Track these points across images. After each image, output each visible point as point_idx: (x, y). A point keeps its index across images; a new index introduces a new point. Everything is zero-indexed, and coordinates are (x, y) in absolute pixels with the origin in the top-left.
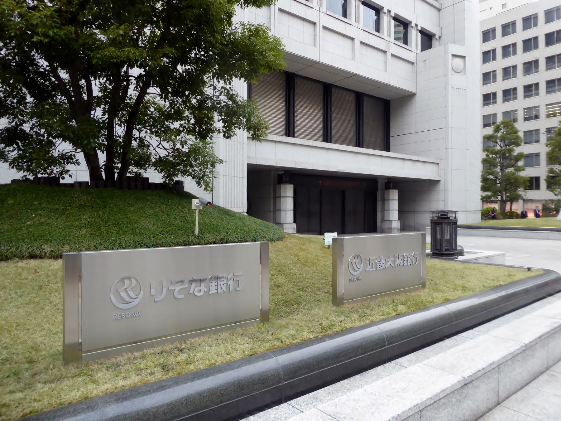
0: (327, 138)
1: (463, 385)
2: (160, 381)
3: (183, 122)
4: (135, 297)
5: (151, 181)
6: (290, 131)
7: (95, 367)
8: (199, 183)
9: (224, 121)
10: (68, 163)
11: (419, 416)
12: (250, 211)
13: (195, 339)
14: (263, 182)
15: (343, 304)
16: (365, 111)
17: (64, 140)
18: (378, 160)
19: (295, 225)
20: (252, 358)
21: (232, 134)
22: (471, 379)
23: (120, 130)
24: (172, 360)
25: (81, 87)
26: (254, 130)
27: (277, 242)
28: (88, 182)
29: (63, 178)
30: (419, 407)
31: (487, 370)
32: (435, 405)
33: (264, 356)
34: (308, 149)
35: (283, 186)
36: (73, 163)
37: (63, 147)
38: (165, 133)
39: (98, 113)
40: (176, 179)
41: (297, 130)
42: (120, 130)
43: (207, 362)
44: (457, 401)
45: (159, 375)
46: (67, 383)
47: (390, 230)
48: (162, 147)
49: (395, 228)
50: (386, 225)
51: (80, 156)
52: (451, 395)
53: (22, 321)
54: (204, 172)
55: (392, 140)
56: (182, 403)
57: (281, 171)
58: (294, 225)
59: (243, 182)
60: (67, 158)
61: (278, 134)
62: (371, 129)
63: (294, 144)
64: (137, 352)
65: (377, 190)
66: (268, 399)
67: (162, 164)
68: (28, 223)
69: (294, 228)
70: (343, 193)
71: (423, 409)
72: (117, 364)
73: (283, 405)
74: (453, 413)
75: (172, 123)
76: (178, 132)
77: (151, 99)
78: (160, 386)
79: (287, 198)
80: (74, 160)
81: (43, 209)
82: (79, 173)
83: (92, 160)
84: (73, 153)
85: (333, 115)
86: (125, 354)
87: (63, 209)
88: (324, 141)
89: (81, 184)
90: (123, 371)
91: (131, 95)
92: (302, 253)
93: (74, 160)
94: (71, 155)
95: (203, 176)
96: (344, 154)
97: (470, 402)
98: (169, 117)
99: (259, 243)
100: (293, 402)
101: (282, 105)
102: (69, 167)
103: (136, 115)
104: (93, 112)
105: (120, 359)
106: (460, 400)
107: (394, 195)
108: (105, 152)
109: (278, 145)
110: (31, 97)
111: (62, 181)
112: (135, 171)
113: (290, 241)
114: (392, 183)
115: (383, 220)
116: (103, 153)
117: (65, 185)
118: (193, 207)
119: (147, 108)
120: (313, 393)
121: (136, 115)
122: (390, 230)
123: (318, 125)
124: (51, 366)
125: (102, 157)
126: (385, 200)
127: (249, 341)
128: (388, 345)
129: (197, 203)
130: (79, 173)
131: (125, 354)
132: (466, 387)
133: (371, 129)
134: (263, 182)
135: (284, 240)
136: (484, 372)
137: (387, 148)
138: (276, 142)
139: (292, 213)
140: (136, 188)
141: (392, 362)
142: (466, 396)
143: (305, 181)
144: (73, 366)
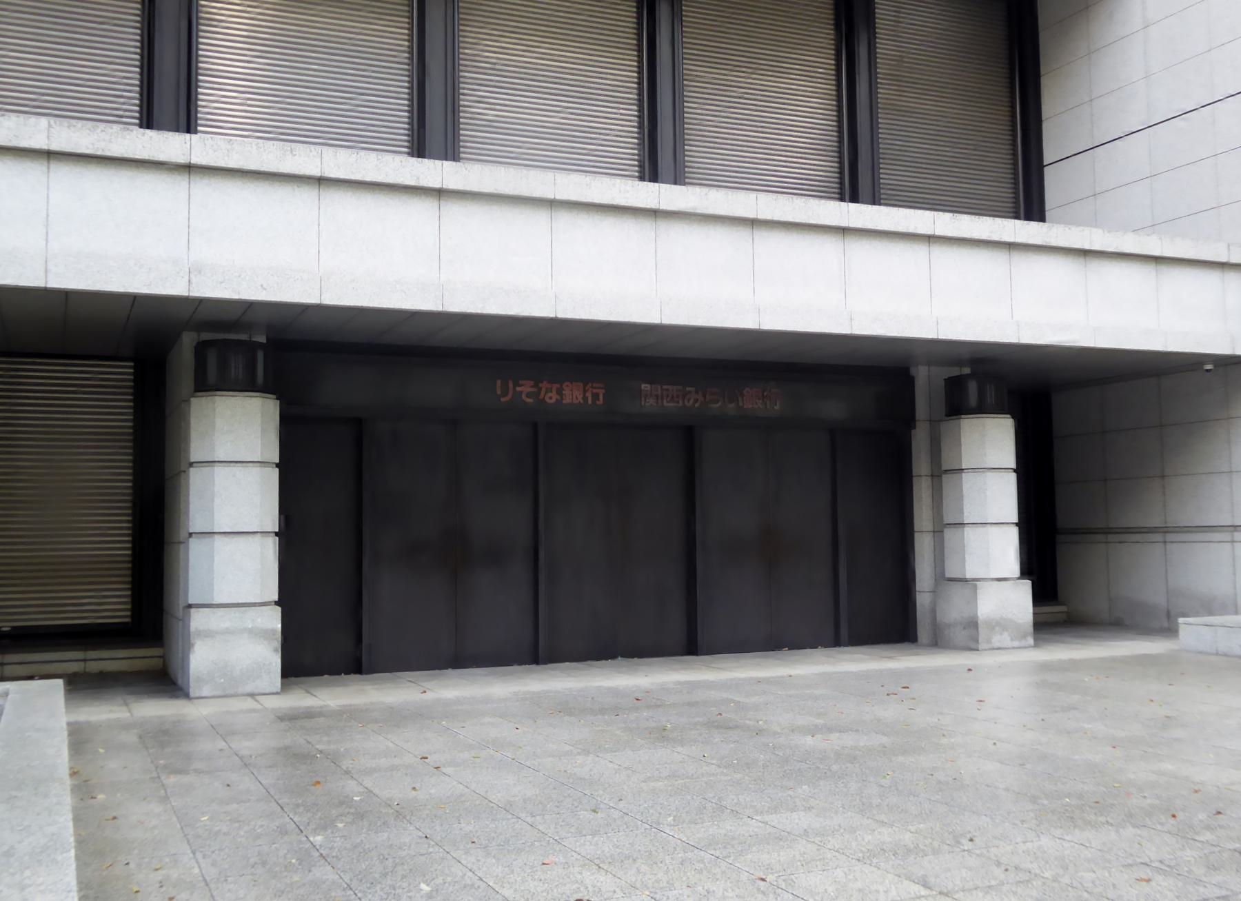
0: (852, 187)
16: (885, 47)
34: (305, 197)
47: (970, 636)
49: (999, 625)
50: (953, 609)
55: (1052, 178)
57: (960, 363)
58: (1026, 587)
63: (440, 193)
79: (219, 471)
96: (564, 219)
109: (63, 174)
115: (943, 579)
122: (970, 636)
126: (944, 473)
137: (1031, 205)
138: (49, 155)
139: (1012, 537)
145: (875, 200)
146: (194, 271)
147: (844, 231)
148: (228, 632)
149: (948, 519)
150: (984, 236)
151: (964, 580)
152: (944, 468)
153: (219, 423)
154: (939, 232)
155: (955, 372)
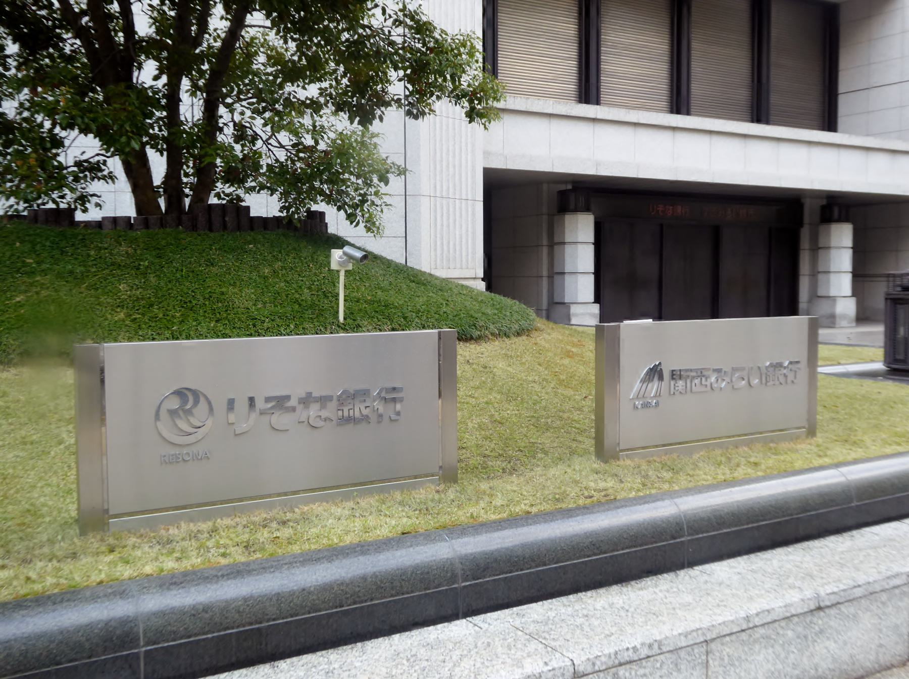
0: (679, 103)
1: (813, 607)
2: (235, 565)
3: (325, 85)
4: (201, 424)
5: (253, 213)
6: (588, 89)
7: (133, 540)
8: (351, 217)
9: (410, 79)
10: (93, 179)
11: (703, 650)
12: (489, 277)
13: (311, 506)
14: (519, 210)
15: (616, 457)
16: (774, 33)
17: (85, 131)
18: (802, 152)
19: (597, 306)
20: (405, 537)
21: (427, 110)
22: (834, 599)
23: (191, 109)
24: (263, 535)
25: (111, 17)
26: (471, 102)
27: (515, 340)
28: (129, 218)
29: (85, 211)
30: (704, 634)
31: (878, 588)
32: (744, 636)
33: (429, 537)
34: (628, 131)
35: (569, 219)
36: (104, 178)
37: (80, 146)
38: (281, 113)
39: (147, 74)
40: (314, 208)
41: (607, 83)
42: (191, 109)
43: (325, 541)
44: (798, 637)
45: (239, 556)
46: (86, 560)
48: (277, 145)
49: (844, 317)
51: (115, 165)
52: (783, 624)
53: (11, 471)
54: (364, 195)
56: (271, 599)
57: (566, 182)
58: (596, 309)
59: (474, 214)
60: (91, 169)
61: (559, 96)
62: (789, 75)
63: (594, 120)
64: (204, 521)
65: (801, 224)
66: (431, 611)
67: (283, 179)
68: (18, 299)
69: (576, 315)
70: (716, 233)
71: (713, 640)
72: (168, 539)
73: (457, 622)
74: (787, 658)
75: (304, 88)
76: (315, 106)
77: (259, 35)
78: (237, 572)
79: (580, 246)
80: (105, 173)
81: (44, 272)
82: (115, 199)
83: (137, 171)
84: (101, 158)
85: (695, 45)
86: (183, 524)
87: (82, 273)
88: (672, 112)
89: (115, 220)
90: (177, 548)
91: (215, 30)
92: (566, 361)
93: (105, 173)
94: (99, 161)
95: (363, 201)
96: (716, 139)
97: (831, 645)
98: (292, 73)
99: (436, 331)
100: (478, 619)
101: (569, 28)
102: (95, 187)
103: (225, 71)
104: (136, 74)
105: (173, 531)
106: (806, 637)
107: (841, 240)
108: (165, 153)
110: (14, 43)
111: (79, 216)
112: (228, 191)
113: (547, 337)
114: (837, 206)
115: (815, 296)
116: (162, 155)
117: (87, 224)
118: (334, 266)
119: (250, 57)
120: (520, 608)
121: (225, 71)
123: (658, 72)
124: (59, 537)
125: (158, 165)
127: (411, 513)
128: (689, 535)
129: (340, 258)
130: (115, 199)
131: (183, 524)
132: (822, 614)
133: (789, 75)
134: (519, 210)
135: (535, 334)
136: (871, 589)
137: (830, 123)
139: (591, 279)
140: (225, 227)
141: (696, 568)
142: (821, 631)
143: (622, 206)
144: (94, 537)
145: (767, 122)
146: (598, 164)
147: (674, 129)
148: (583, 314)
149: (557, 270)
150: (838, 142)
151: (564, 303)
152: (820, 245)
153: (579, 225)
154: (599, 117)
155: (563, 187)
